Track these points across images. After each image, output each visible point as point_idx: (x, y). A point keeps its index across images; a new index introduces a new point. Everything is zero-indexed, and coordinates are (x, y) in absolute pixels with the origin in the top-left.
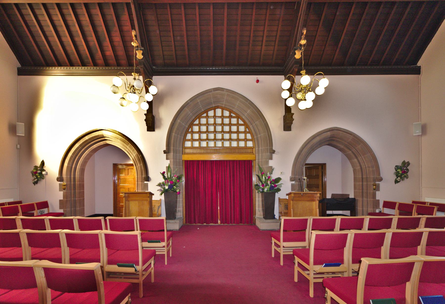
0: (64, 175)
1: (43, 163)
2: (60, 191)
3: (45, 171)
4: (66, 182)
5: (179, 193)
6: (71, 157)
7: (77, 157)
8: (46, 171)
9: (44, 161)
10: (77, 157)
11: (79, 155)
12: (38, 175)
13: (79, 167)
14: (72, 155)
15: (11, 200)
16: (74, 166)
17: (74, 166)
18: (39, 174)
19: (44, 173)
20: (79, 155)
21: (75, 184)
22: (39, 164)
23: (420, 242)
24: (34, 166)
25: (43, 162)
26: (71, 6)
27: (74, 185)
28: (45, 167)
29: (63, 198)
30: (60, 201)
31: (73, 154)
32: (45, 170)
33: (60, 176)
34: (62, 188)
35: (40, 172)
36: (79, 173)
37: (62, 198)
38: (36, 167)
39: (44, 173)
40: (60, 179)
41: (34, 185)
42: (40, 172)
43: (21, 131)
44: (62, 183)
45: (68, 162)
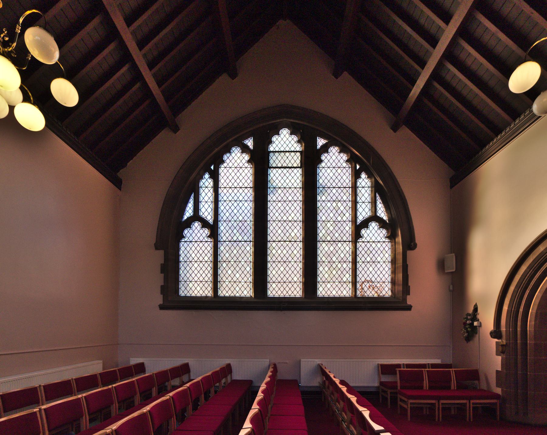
0: (503, 329)
1: (476, 309)
2: (497, 355)
3: (478, 320)
4: (506, 340)
5: (472, 383)
6: (515, 292)
7: (528, 292)
8: (480, 321)
9: (477, 305)
10: (528, 292)
11: (530, 287)
12: (469, 328)
13: (535, 311)
14: (517, 290)
15: (438, 361)
16: (521, 310)
17: (521, 310)
18: (469, 326)
19: (475, 324)
20: (530, 287)
21: (526, 344)
22: (471, 310)
23: (473, 48)
24: (467, 313)
25: (476, 307)
26: (486, 17)
27: (525, 344)
28: (479, 315)
29: (502, 368)
30: (497, 372)
31: (518, 286)
32: (479, 319)
33: (495, 329)
34: (501, 350)
35: (470, 322)
36: (533, 323)
37: (500, 369)
38: (468, 314)
39: (475, 324)
40: (496, 334)
41: (466, 342)
42: (470, 322)
43: (451, 265)
44: (500, 341)
45: (508, 303)
